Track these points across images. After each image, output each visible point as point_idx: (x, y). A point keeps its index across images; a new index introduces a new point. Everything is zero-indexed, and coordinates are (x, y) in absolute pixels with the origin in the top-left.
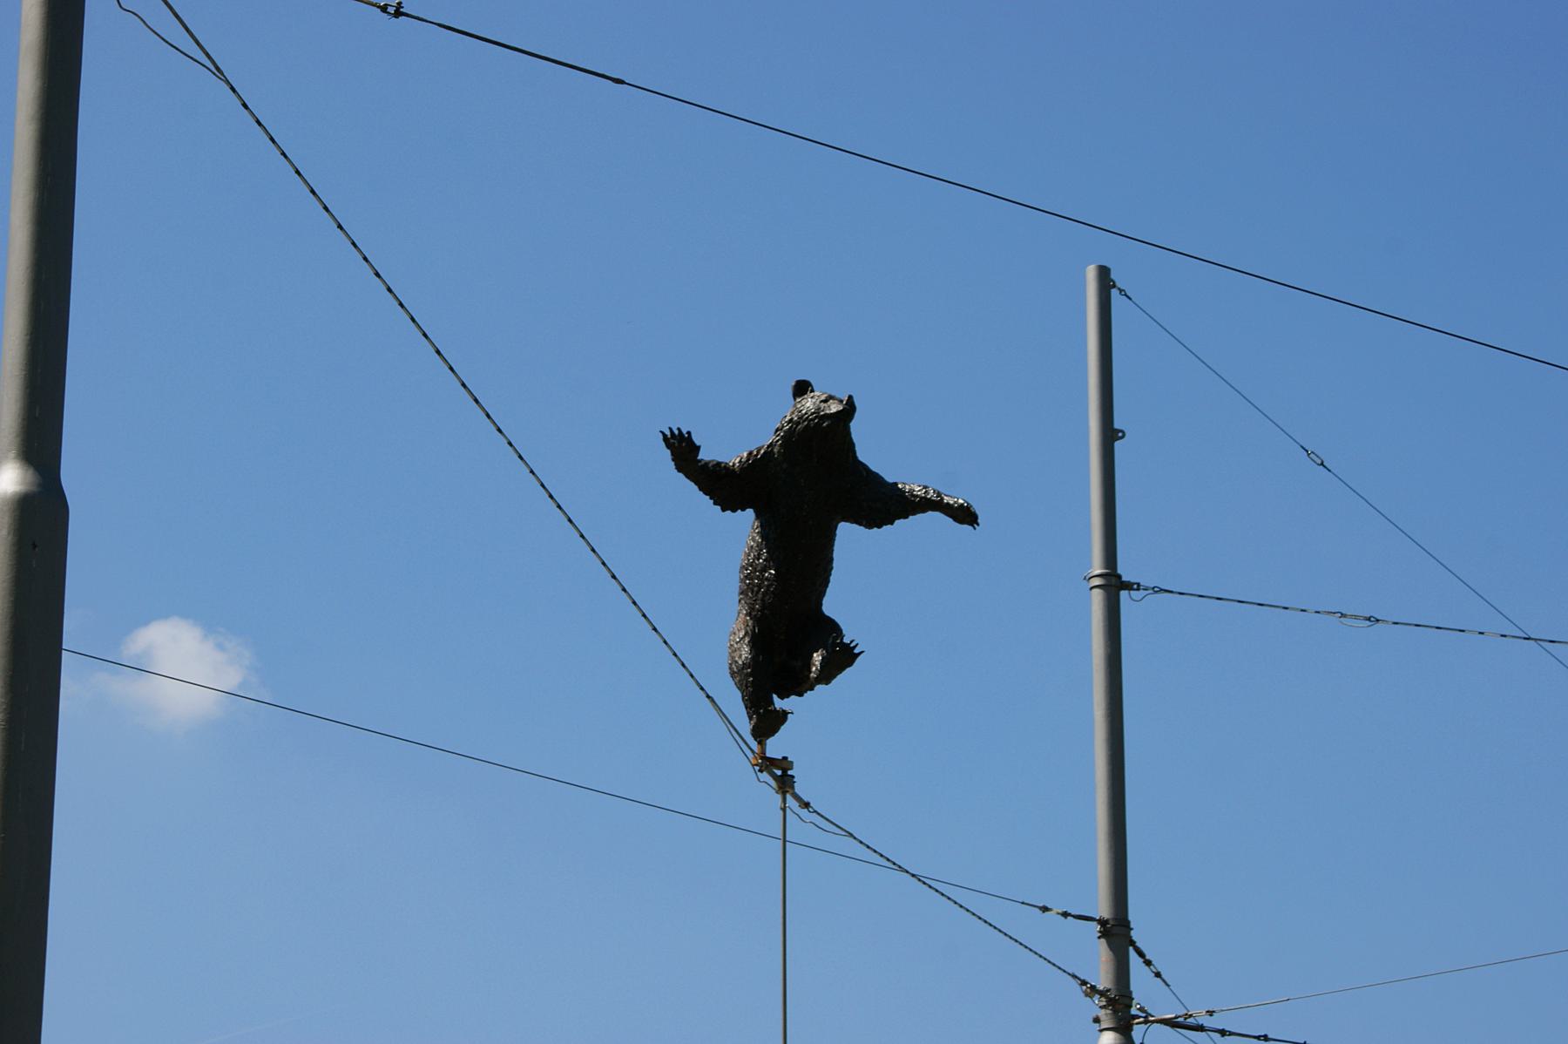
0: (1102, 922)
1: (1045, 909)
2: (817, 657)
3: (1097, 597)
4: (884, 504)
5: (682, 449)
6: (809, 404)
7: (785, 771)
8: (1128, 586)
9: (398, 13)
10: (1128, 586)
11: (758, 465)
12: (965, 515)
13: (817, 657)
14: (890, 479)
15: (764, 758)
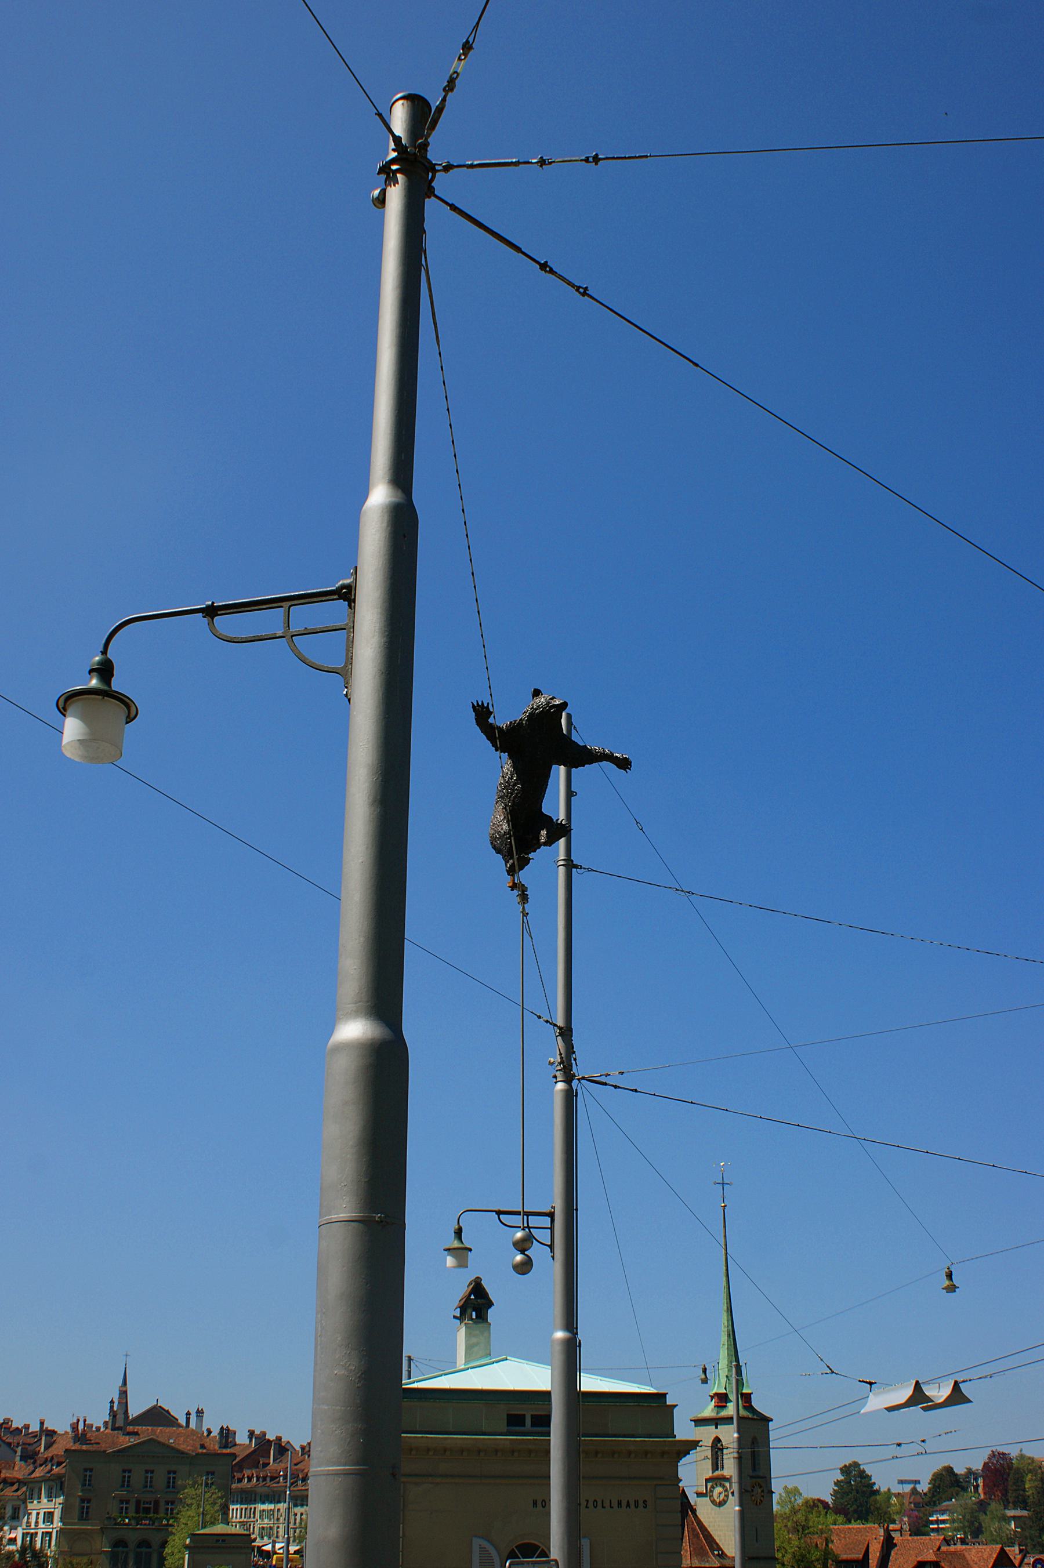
0: (560, 1028)
1: (539, 1017)
2: (544, 833)
3: (562, 870)
4: (579, 756)
5: (482, 713)
6: (542, 700)
7: (523, 892)
8: (576, 866)
9: (585, 294)
10: (576, 866)
11: (515, 728)
12: (624, 764)
13: (544, 833)
14: (582, 744)
15: (514, 883)
